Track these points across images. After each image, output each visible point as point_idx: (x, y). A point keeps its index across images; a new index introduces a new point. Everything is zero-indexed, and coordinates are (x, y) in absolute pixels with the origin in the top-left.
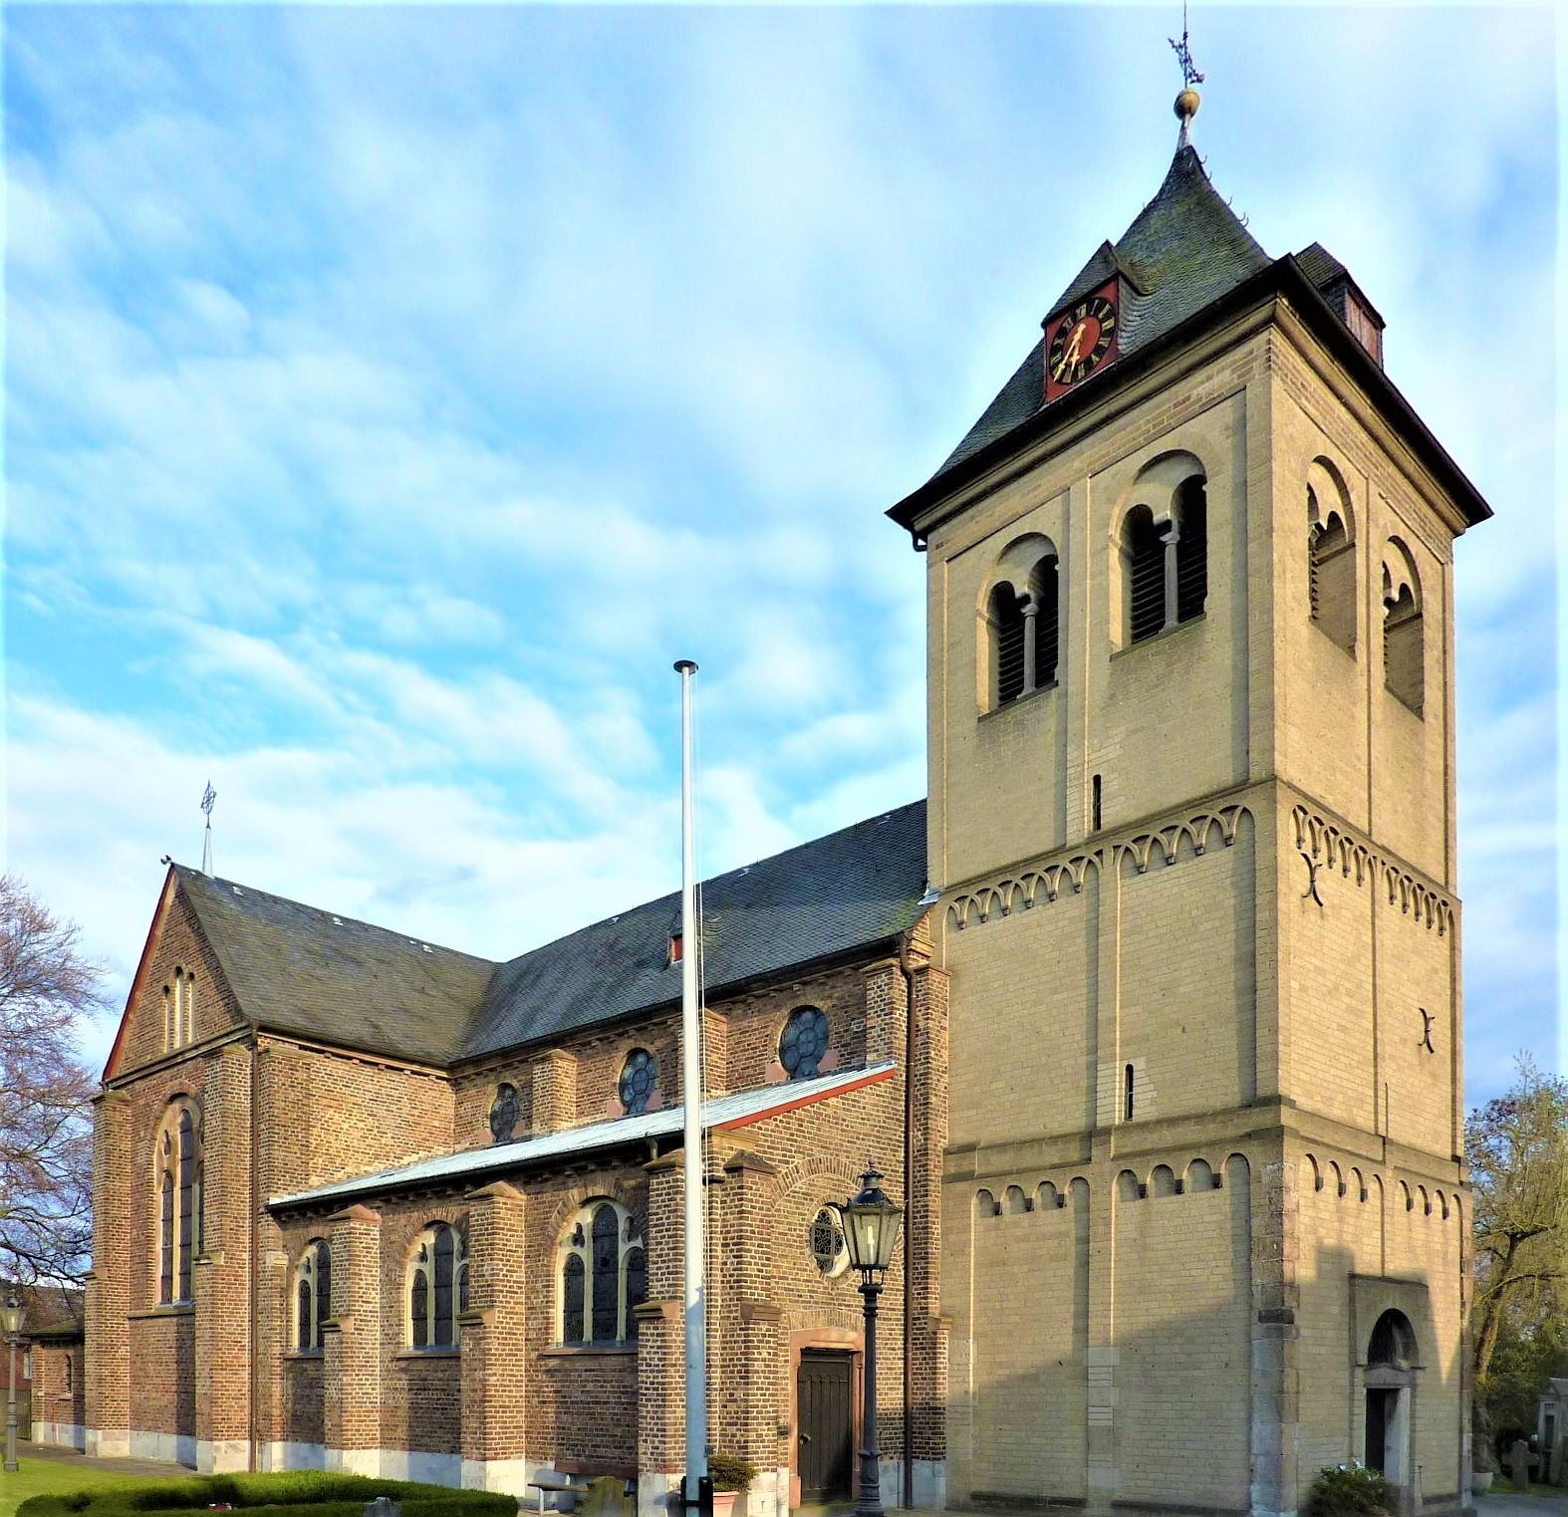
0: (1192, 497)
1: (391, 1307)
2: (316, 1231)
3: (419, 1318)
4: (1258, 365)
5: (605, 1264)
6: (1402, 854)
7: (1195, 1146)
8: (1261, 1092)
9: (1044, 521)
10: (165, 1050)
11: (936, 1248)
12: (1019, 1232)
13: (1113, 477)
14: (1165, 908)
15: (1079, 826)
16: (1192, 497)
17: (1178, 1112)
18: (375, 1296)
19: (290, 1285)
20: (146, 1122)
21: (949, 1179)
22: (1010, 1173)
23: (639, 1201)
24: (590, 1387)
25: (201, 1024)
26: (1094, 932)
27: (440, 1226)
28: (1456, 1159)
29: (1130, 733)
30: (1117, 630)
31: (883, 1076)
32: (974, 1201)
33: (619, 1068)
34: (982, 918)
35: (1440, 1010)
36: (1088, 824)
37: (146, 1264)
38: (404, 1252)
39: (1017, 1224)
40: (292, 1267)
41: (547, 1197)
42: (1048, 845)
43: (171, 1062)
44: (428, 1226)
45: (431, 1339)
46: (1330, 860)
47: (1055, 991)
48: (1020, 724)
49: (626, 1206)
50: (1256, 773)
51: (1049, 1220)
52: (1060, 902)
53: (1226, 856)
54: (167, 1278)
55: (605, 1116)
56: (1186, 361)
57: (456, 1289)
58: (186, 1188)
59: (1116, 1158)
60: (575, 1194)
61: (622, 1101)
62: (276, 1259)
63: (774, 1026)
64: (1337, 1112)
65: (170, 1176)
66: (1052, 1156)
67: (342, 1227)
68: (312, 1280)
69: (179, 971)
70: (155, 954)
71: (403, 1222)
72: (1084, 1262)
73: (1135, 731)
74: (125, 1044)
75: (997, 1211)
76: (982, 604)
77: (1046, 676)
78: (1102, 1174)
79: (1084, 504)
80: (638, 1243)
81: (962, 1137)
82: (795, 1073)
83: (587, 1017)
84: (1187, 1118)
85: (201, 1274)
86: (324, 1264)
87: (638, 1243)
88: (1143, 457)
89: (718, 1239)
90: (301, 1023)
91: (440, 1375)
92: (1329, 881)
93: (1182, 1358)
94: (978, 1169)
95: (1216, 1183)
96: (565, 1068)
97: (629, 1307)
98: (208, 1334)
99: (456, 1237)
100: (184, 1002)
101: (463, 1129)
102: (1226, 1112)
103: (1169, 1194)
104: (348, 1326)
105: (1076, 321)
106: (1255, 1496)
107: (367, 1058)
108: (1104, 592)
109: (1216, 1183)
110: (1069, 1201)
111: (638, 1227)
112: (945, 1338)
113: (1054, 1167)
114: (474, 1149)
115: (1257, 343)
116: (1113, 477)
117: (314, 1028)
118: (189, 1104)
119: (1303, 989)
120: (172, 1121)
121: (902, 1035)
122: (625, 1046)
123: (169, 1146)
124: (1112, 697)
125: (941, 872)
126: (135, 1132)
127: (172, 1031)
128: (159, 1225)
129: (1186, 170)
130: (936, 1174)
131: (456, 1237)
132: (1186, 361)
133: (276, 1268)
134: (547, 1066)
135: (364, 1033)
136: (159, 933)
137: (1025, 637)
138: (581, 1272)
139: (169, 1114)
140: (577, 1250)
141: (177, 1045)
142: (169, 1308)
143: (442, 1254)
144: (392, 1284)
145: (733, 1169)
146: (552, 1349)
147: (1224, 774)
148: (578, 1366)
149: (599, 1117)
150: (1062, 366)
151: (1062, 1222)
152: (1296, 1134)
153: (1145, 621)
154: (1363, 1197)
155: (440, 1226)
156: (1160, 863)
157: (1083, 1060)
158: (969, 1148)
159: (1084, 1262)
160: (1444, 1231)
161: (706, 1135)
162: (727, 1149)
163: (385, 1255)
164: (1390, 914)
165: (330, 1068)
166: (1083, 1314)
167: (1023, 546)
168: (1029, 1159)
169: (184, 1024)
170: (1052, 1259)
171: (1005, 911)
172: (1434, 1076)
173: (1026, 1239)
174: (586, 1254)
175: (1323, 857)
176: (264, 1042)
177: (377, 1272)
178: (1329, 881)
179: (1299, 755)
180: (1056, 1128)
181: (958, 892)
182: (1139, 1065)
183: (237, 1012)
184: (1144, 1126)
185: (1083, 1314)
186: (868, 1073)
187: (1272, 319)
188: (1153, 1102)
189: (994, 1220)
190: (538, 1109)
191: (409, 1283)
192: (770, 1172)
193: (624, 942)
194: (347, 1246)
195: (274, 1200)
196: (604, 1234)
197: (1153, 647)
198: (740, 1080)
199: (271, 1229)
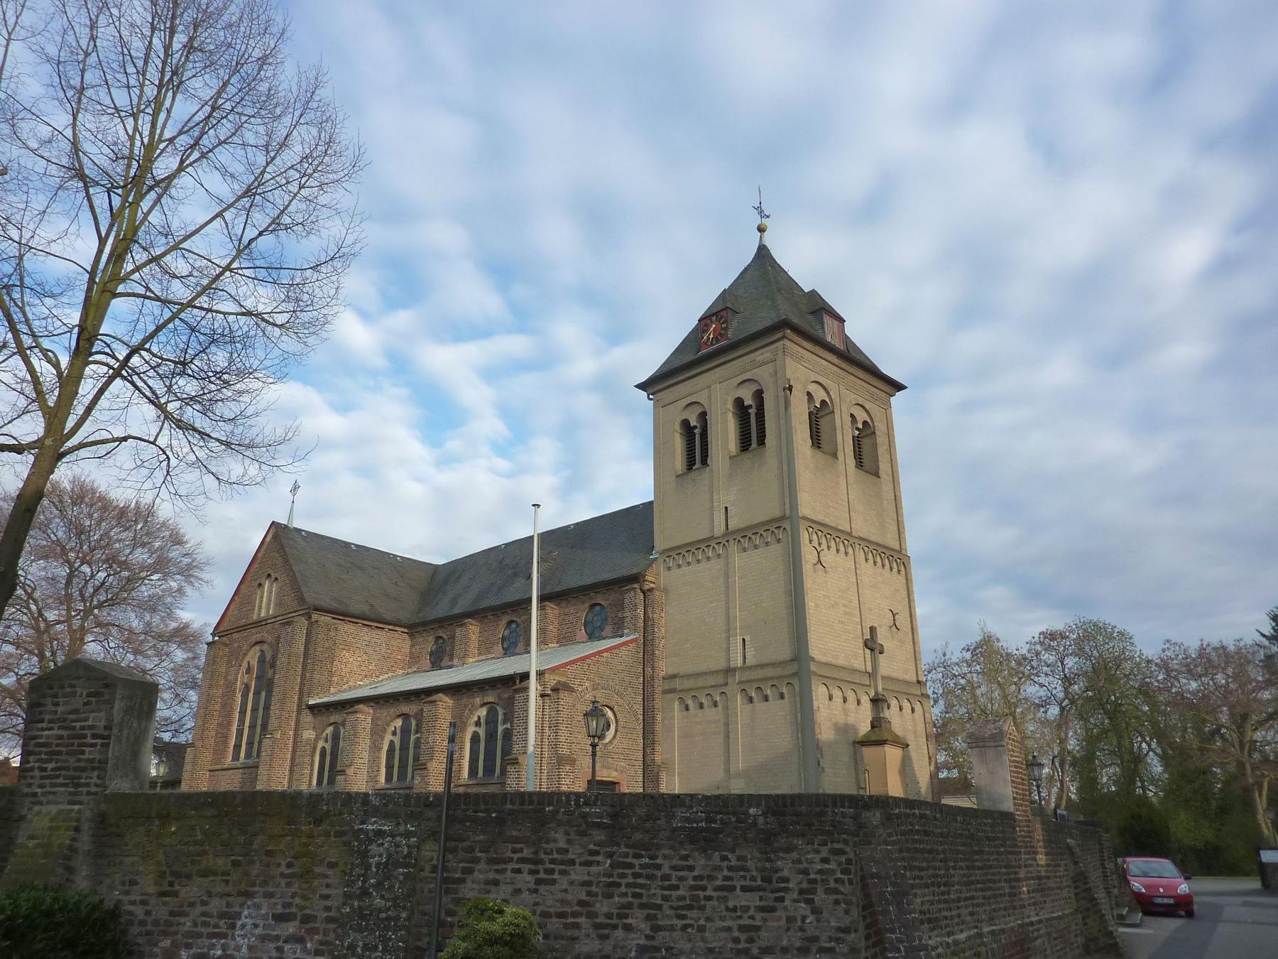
0: (759, 395)
1: (374, 762)
2: (333, 718)
3: (389, 767)
4: (780, 353)
5: (491, 735)
6: (872, 539)
7: (772, 678)
9: (701, 397)
10: (255, 617)
11: (658, 728)
14: (756, 566)
15: (719, 529)
16: (759, 395)
17: (765, 661)
18: (366, 755)
19: (315, 749)
20: (237, 655)
21: (665, 692)
23: (509, 705)
25: (279, 604)
26: (727, 576)
27: (405, 717)
28: (919, 682)
30: (733, 446)
31: (631, 641)
32: (677, 703)
33: (502, 631)
34: (679, 566)
35: (902, 609)
36: (723, 528)
37: (226, 738)
38: (384, 730)
40: (317, 739)
41: (464, 701)
42: (707, 535)
43: (259, 623)
44: (399, 716)
45: (395, 778)
46: (829, 548)
49: (503, 708)
51: (710, 712)
53: (778, 546)
54: (237, 747)
56: (753, 347)
57: (411, 751)
58: (257, 693)
59: (740, 682)
60: (478, 701)
62: (308, 734)
63: (580, 612)
64: (841, 662)
65: (247, 687)
66: (711, 681)
67: (352, 717)
68: (328, 747)
69: (269, 575)
70: (256, 565)
72: (727, 736)
74: (230, 613)
75: (687, 708)
76: (678, 428)
77: (704, 462)
79: (718, 393)
80: (508, 726)
81: (671, 671)
82: (592, 637)
83: (486, 603)
85: (266, 742)
86: (336, 737)
87: (508, 726)
89: (546, 725)
90: (334, 605)
92: (828, 557)
94: (678, 687)
96: (473, 630)
97: (502, 759)
98: (265, 778)
99: (414, 722)
100: (270, 592)
101: (414, 659)
104: (350, 771)
105: (712, 322)
108: (726, 431)
109: (782, 696)
110: (720, 704)
111: (508, 718)
112: (663, 776)
115: (779, 344)
117: (341, 608)
118: (265, 647)
119: (817, 605)
120: (253, 657)
121: (641, 621)
122: (505, 619)
123: (249, 671)
125: (660, 544)
126: (229, 662)
127: (260, 607)
128: (237, 715)
129: (763, 253)
130: (658, 690)
131: (414, 722)
132: (753, 347)
133: (308, 740)
134: (463, 629)
135: (365, 609)
137: (695, 444)
138: (479, 741)
139: (252, 652)
140: (477, 729)
141: (263, 615)
142: (237, 764)
143: (405, 731)
144: (375, 748)
145: (555, 690)
152: (816, 674)
153: (745, 444)
154: (859, 703)
155: (405, 717)
157: (724, 635)
158: (674, 677)
159: (727, 736)
160: (914, 720)
161: (540, 674)
162: (552, 680)
163: (373, 732)
164: (867, 569)
165: (348, 628)
166: (728, 762)
168: (701, 682)
169: (269, 604)
171: (689, 564)
172: (901, 641)
174: (482, 732)
175: (824, 546)
176: (315, 617)
177: (368, 741)
178: (829, 557)
179: (808, 505)
181: (668, 552)
183: (301, 600)
184: (750, 668)
185: (728, 762)
186: (624, 639)
187: (784, 337)
190: (457, 651)
191: (385, 747)
192: (571, 690)
193: (507, 561)
194: (354, 727)
195: (311, 702)
196: (491, 721)
197: (747, 455)
198: (565, 639)
199: (307, 718)
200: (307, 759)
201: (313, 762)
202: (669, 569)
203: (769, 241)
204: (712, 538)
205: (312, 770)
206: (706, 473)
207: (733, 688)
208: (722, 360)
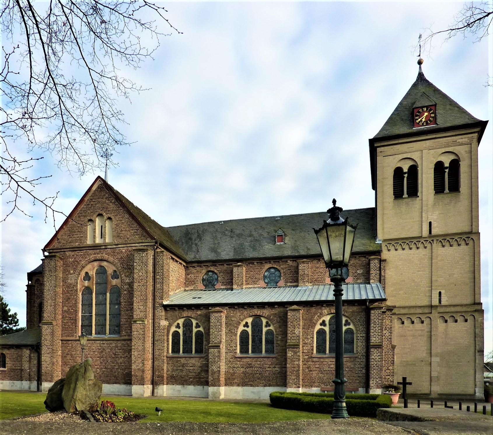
8: (476, 301)
9: (415, 156)
12: (409, 329)
13: (435, 152)
22: (407, 314)
29: (440, 214)
39: (409, 327)
47: (419, 271)
48: (407, 204)
50: (474, 231)
52: (420, 250)
55: (259, 286)
61: (265, 282)
62: (164, 323)
71: (239, 314)
73: (441, 214)
78: (435, 317)
84: (458, 305)
88: (444, 150)
91: (259, 363)
93: (457, 360)
95: (466, 321)
102: (466, 305)
103: (453, 322)
106: (477, 391)
107: (174, 257)
113: (420, 314)
114: (196, 290)
116: (435, 152)
124: (435, 204)
129: (421, 76)
136: (86, 199)
146: (314, 355)
147: (467, 229)
148: (326, 360)
149: (256, 286)
150: (419, 120)
151: (425, 327)
156: (449, 246)
167: (406, 160)
168: (412, 311)
170: (419, 336)
173: (412, 331)
180: (419, 304)
182: (443, 292)
188: (447, 301)
189: (401, 325)
195: (165, 303)
199: (161, 312)
200: (165, 338)
201: (168, 339)
202: (389, 250)
203: (424, 71)
204: (421, 237)
205: (168, 344)
206: (417, 201)
207: (435, 315)
208: (434, 136)
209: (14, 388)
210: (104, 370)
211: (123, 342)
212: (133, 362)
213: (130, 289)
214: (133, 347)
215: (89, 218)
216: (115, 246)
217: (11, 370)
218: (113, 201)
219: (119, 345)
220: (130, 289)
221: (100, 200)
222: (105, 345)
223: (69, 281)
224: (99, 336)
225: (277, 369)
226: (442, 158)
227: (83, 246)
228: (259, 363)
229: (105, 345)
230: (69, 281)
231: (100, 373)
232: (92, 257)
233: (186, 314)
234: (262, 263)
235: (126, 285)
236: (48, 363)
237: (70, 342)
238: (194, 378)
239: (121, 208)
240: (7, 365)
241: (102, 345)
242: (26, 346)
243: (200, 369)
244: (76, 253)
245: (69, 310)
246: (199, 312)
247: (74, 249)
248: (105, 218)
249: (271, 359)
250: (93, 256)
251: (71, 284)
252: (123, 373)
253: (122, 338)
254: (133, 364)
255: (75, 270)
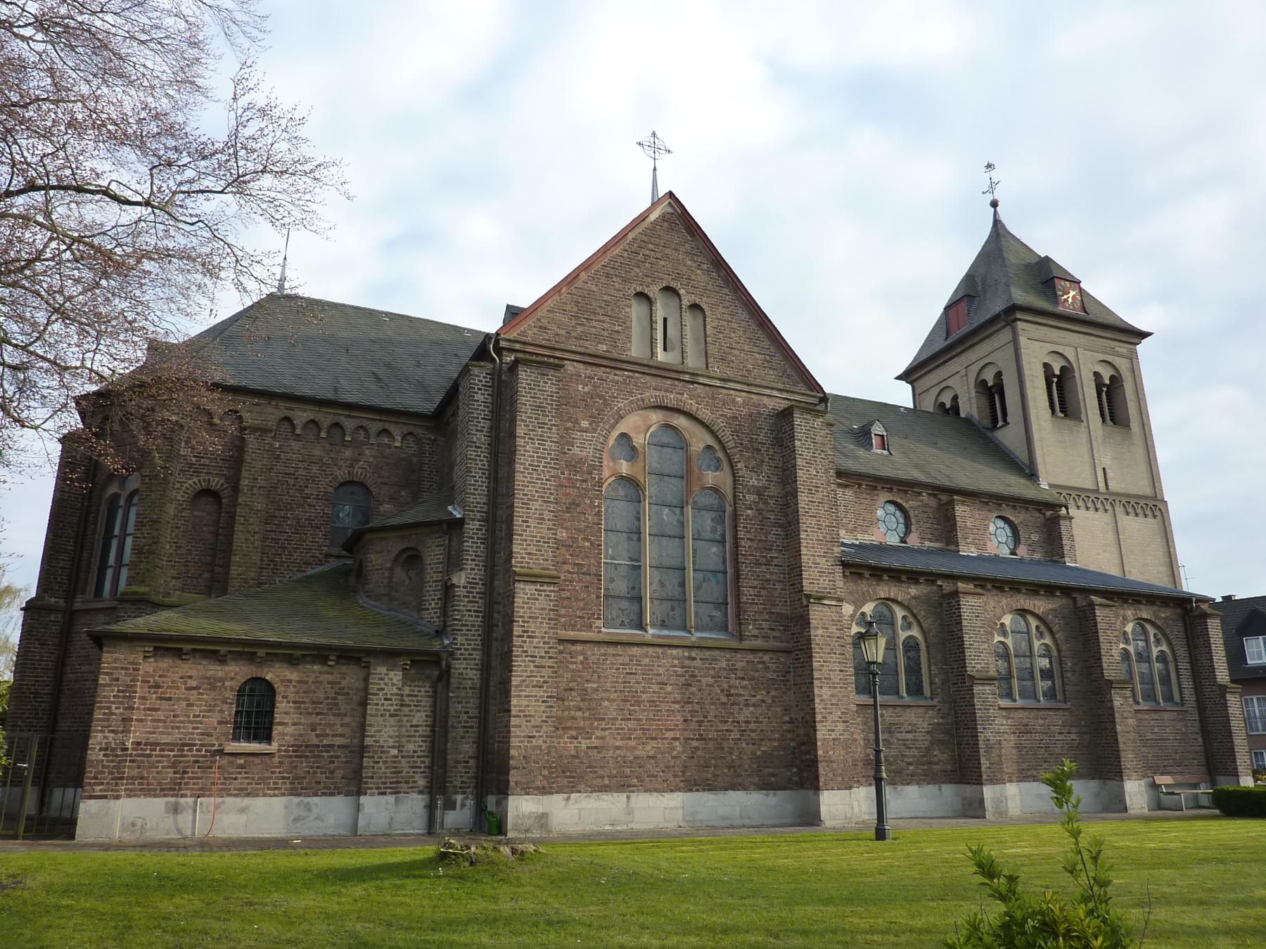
9: (1069, 353)
24: (1156, 730)
60: (1129, 613)
71: (992, 604)
91: (1041, 722)
129: (997, 222)
209: (312, 828)
210: (695, 744)
211: (751, 657)
212: (818, 718)
213: (761, 506)
214: (816, 675)
215: (639, 289)
216: (718, 383)
217: (300, 749)
218: (705, 267)
219: (740, 665)
220: (761, 506)
221: (668, 251)
222: (698, 663)
223: (576, 450)
224: (665, 632)
225: (1073, 736)
226: (1101, 369)
227: (623, 357)
228: (1041, 722)
229: (698, 663)
230: (576, 450)
231: (684, 757)
232: (650, 395)
233: (884, 590)
234: (875, 488)
235: (749, 492)
236: (536, 721)
237: (579, 648)
238: (919, 763)
239: (726, 291)
240: (277, 730)
241: (687, 662)
242: (390, 655)
243: (928, 737)
244: (600, 372)
245: (575, 540)
246: (913, 591)
247: (593, 360)
248: (685, 302)
249: (1060, 713)
250: (654, 393)
251: (581, 461)
252: (753, 753)
253: (747, 644)
254: (819, 726)
255: (594, 420)
